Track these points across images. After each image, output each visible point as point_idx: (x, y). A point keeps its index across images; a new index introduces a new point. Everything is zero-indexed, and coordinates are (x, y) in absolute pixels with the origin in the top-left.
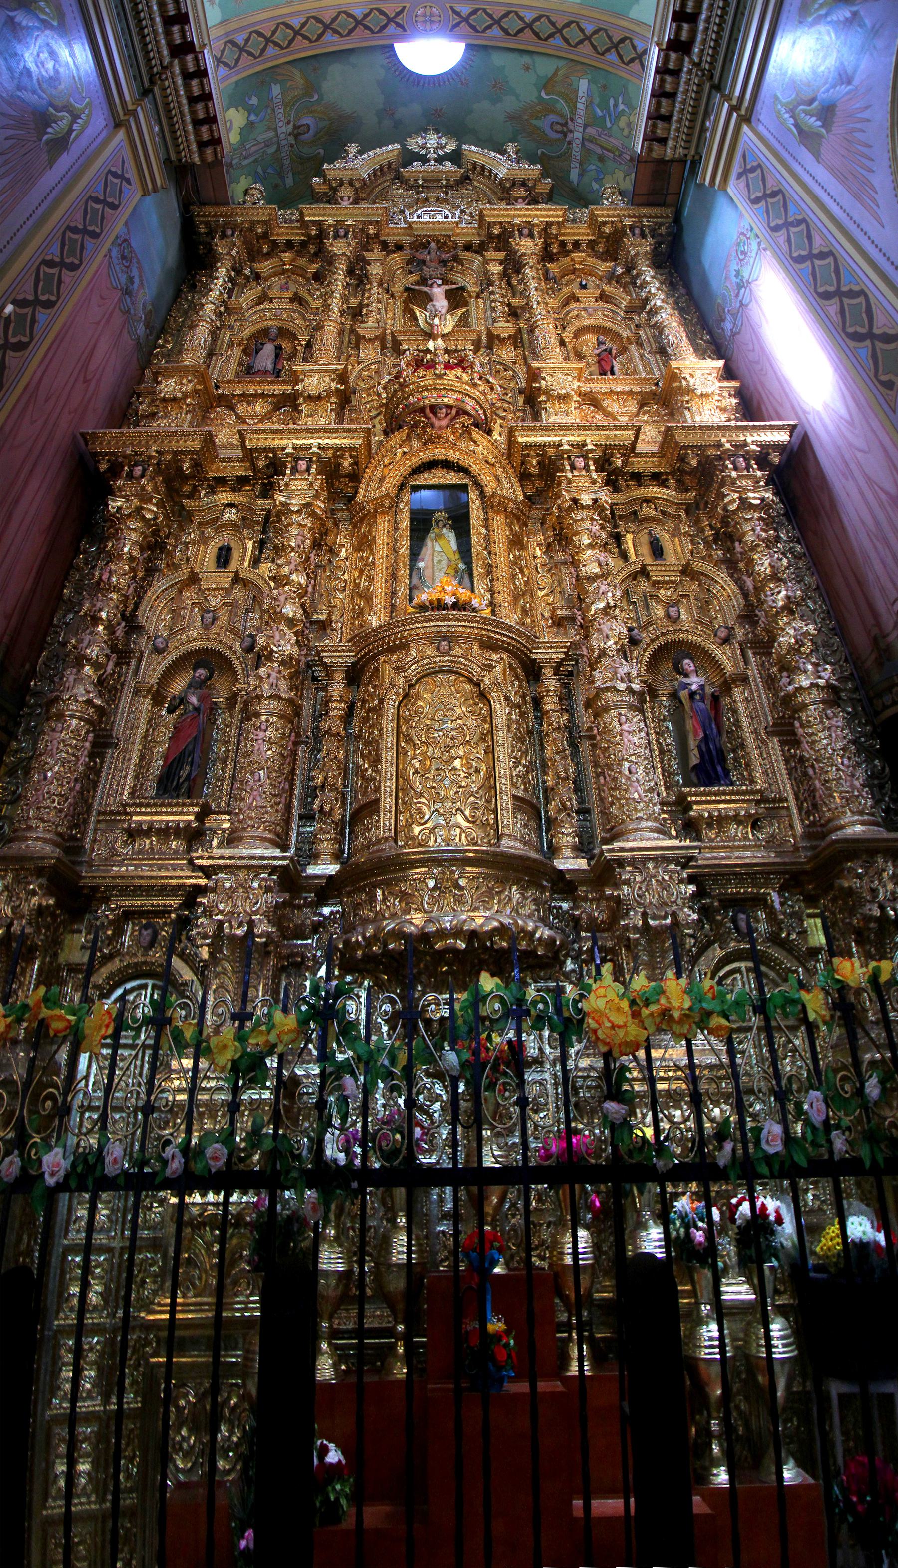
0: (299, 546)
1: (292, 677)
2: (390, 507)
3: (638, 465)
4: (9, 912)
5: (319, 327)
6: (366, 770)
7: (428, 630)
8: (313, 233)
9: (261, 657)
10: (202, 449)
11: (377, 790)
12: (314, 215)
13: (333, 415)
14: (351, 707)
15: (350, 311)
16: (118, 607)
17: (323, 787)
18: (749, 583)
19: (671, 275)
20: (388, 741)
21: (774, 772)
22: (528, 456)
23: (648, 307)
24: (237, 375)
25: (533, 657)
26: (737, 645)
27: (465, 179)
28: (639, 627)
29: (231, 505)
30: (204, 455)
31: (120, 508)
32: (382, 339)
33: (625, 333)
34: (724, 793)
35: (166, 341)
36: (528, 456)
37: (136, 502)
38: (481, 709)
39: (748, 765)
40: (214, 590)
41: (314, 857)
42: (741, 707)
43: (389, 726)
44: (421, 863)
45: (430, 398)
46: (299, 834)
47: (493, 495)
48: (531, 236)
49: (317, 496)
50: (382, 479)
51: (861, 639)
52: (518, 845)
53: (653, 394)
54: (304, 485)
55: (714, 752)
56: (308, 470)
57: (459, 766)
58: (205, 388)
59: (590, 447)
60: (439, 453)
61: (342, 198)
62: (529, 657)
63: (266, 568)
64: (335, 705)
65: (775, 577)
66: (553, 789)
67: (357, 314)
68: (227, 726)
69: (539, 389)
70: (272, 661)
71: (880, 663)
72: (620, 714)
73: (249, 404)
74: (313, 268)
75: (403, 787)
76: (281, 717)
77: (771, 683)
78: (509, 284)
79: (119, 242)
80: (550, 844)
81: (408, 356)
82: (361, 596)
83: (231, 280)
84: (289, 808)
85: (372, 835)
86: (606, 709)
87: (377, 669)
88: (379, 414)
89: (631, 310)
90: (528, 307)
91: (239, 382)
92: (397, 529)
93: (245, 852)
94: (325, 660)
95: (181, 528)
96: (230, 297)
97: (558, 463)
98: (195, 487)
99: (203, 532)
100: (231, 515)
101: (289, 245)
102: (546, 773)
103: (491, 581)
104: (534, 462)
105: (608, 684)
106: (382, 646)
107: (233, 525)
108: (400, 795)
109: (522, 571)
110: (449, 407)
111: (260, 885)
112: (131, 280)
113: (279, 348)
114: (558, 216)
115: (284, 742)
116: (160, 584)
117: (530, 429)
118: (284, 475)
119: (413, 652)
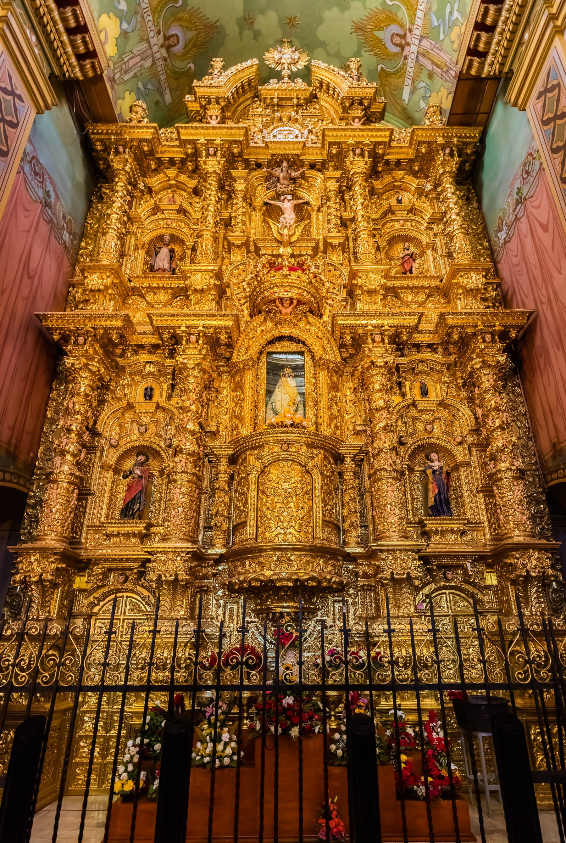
1: (195, 461)
2: (253, 366)
3: (419, 338)
4: (40, 570)
5: (199, 236)
8: (189, 151)
9: (177, 451)
10: (124, 326)
11: (246, 516)
12: (188, 134)
13: (214, 303)
14: (232, 477)
15: (223, 222)
16: (82, 423)
17: (216, 514)
18: (480, 412)
19: (469, 190)
20: (252, 495)
21: (478, 510)
22: (345, 333)
23: (445, 219)
24: (144, 271)
25: (340, 452)
26: (467, 446)
27: (313, 98)
28: (407, 435)
29: (150, 362)
30: (126, 329)
31: (73, 365)
32: (246, 244)
33: (425, 240)
34: (446, 520)
35: (87, 244)
36: (345, 333)
37: (83, 360)
39: (463, 506)
40: (145, 413)
41: (213, 545)
42: (463, 478)
43: (253, 487)
44: (270, 550)
45: (279, 293)
46: (204, 535)
47: (321, 358)
48: (362, 155)
49: (204, 358)
50: (247, 349)
51: (546, 445)
52: (325, 542)
53: (438, 288)
54: (196, 352)
55: (443, 501)
56: (197, 342)
57: (293, 506)
58: (121, 282)
59: (386, 328)
60: (285, 331)
61: (211, 117)
62: (337, 452)
63: (176, 401)
64: (222, 475)
65: (497, 409)
67: (228, 223)
69: (356, 285)
70: (183, 454)
71: (554, 457)
73: (155, 293)
74: (192, 183)
75: (260, 515)
76: (189, 482)
77: (484, 466)
78: (343, 199)
79: (28, 158)
80: (344, 541)
81: (264, 260)
82: (236, 418)
83: (129, 193)
84: (197, 523)
85: (244, 536)
86: (380, 479)
87: (246, 458)
89: (433, 221)
90: (353, 220)
91: (146, 277)
92: (258, 379)
95: (118, 376)
96: (130, 208)
97: (364, 338)
98: (123, 350)
99: (133, 379)
100: (150, 368)
101: (172, 162)
102: (343, 509)
103: (317, 410)
104: (348, 337)
105: (383, 467)
107: (153, 375)
108: (259, 519)
109: (336, 404)
110: (291, 300)
111: (181, 560)
112: (47, 193)
113: (172, 251)
114: (385, 136)
116: (107, 411)
117: (347, 315)
119: (267, 449)
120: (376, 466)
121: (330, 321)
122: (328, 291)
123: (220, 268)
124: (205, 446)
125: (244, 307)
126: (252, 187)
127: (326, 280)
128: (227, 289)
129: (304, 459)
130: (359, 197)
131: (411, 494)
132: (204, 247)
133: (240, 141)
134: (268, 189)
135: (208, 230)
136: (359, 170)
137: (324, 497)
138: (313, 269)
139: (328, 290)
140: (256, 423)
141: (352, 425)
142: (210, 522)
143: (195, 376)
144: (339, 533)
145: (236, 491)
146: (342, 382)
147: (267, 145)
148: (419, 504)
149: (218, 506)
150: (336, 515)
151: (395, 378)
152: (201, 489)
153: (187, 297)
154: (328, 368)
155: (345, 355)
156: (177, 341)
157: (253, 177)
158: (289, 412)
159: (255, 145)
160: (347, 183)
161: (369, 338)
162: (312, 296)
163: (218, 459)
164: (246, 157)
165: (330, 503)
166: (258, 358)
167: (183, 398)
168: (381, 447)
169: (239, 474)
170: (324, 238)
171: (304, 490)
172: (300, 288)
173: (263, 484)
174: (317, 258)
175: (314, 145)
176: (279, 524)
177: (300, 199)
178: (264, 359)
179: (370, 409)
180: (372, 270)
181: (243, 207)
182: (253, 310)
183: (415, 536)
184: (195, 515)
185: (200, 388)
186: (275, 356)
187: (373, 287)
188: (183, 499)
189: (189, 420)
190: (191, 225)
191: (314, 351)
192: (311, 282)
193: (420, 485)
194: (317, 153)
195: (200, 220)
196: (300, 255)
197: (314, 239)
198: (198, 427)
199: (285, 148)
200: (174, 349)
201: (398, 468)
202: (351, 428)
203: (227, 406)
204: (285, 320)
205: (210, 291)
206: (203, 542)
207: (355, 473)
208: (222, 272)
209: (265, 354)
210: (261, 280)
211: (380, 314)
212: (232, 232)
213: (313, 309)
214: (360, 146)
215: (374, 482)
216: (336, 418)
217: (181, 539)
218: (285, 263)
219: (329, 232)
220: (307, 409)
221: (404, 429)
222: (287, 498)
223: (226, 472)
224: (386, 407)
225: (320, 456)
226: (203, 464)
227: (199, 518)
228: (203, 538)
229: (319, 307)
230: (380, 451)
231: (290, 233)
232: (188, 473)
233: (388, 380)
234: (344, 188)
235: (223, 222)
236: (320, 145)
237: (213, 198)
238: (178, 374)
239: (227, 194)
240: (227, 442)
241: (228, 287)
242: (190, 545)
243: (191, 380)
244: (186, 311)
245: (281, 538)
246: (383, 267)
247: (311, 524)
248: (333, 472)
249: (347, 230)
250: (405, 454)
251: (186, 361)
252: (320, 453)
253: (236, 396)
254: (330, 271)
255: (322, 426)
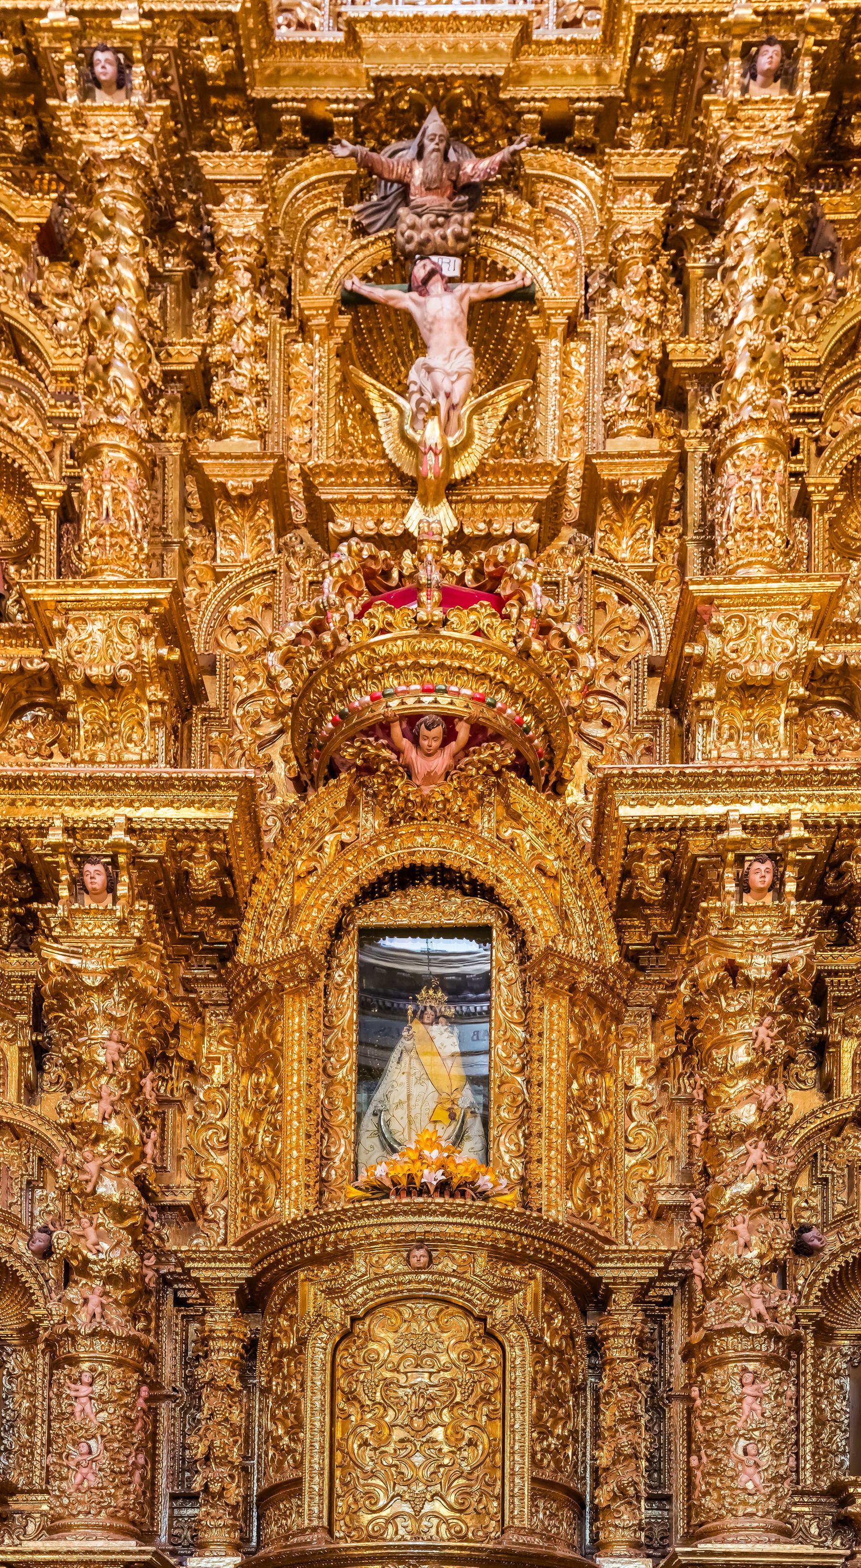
0: (115, 1064)
1: (131, 1302)
6: (280, 1438)
7: (389, 1230)
11: (299, 1465)
13: (161, 734)
14: (251, 1348)
15: (175, 390)
17: (207, 1458)
22: (640, 855)
25: (596, 1274)
28: (825, 1224)
36: (640, 855)
38: (486, 1356)
43: (318, 1379)
46: (172, 1517)
47: (549, 953)
49: (139, 952)
50: (291, 914)
52: (537, 1541)
56: (111, 888)
59: (797, 832)
62: (587, 1276)
64: (220, 1344)
66: (607, 1469)
68: (28, 1371)
69: (700, 662)
72: (745, 1370)
80: (595, 1539)
82: (258, 1162)
84: (151, 1485)
85: (293, 1522)
86: (721, 1362)
87: (293, 1291)
88: (281, 732)
92: (330, 1027)
93: (76, 1545)
94: (193, 1274)
97: (712, 875)
103: (526, 1137)
104: (653, 872)
105: (733, 1323)
106: (302, 1253)
108: (338, 1473)
109: (594, 1116)
110: (449, 721)
115: (126, 1400)
118: (56, 899)
119: (360, 1265)
120: (712, 1321)
121: (590, 809)
122: (589, 689)
123: (178, 594)
124: (162, 1254)
125: (274, 752)
126: (291, 224)
127: (584, 643)
128: (207, 679)
129: (479, 1298)
130: (749, 261)
131: (816, 1406)
132: (107, 503)
133: (230, 17)
134: (360, 231)
135: (119, 428)
136: (761, 146)
137: (540, 1411)
138: (536, 598)
139: (588, 682)
140: (323, 1181)
141: (642, 1187)
142: (189, 1479)
143: (112, 1018)
144: (581, 1517)
145: (266, 1391)
146: (620, 1039)
147: (352, 35)
148: (839, 1437)
149: (210, 1435)
150: (575, 1466)
151: (806, 1025)
152: (155, 1385)
153: (61, 712)
154: (573, 989)
155: (636, 940)
156: (36, 885)
157: (293, 182)
158: (433, 1144)
159: (299, 36)
160: (705, 204)
161: (729, 874)
162: (529, 707)
163: (206, 1292)
164: (260, 92)
165: (558, 1431)
166: (330, 953)
167: (77, 1095)
168: (734, 1259)
169: (273, 1340)
170: (588, 460)
171: (478, 1391)
172: (484, 676)
173: (349, 1372)
174: (552, 550)
175: (569, 35)
176: (399, 1489)
177: (501, 274)
178: (349, 954)
179: (708, 1135)
180: (769, 599)
181: (257, 320)
182: (305, 765)
183: (814, 1530)
184: (141, 1460)
185: (134, 1057)
186: (389, 943)
187: (766, 670)
188: (103, 1415)
189: (102, 1169)
190: (47, 401)
191: (526, 926)
192: (525, 653)
193: (847, 1383)
194: (580, 72)
195: (82, 381)
196: (489, 540)
197: (546, 467)
198: (135, 1191)
199: (434, 51)
200: (31, 915)
201: (784, 1327)
202: (638, 1197)
203: (225, 1122)
204: (425, 804)
205: (143, 686)
206: (171, 1536)
207: (640, 1341)
208: (183, 609)
209: (354, 934)
210: (337, 642)
211: (780, 778)
212: (218, 435)
213: (531, 757)
214: (783, 33)
215: (701, 1369)
216: (592, 1162)
217: (104, 1528)
218: (430, 574)
219: (610, 432)
220: (493, 1133)
221: (815, 1201)
222: (423, 1413)
223: (230, 1336)
224: (762, 1129)
225: (534, 1288)
226: (157, 1308)
227: (154, 1470)
228: (170, 1526)
229: (551, 750)
230: (730, 1273)
231: (452, 442)
232: (111, 1336)
233: (782, 1035)
234: (688, 224)
235: (175, 390)
236: (596, 34)
237: (128, 275)
238: (51, 1009)
239: (187, 255)
240: (231, 1240)
241: (213, 672)
242: (131, 1544)
243: (100, 1030)
244: (59, 765)
245: (404, 1527)
246: (811, 587)
247: (497, 1490)
248: (571, 1337)
249: (683, 424)
250: (811, 1286)
251: (76, 962)
252: (532, 1277)
253: (257, 1087)
254: (602, 606)
255: (544, 1192)
